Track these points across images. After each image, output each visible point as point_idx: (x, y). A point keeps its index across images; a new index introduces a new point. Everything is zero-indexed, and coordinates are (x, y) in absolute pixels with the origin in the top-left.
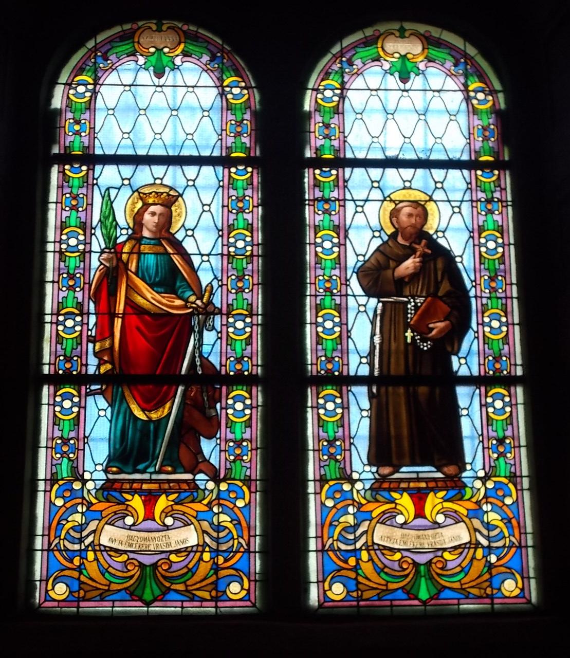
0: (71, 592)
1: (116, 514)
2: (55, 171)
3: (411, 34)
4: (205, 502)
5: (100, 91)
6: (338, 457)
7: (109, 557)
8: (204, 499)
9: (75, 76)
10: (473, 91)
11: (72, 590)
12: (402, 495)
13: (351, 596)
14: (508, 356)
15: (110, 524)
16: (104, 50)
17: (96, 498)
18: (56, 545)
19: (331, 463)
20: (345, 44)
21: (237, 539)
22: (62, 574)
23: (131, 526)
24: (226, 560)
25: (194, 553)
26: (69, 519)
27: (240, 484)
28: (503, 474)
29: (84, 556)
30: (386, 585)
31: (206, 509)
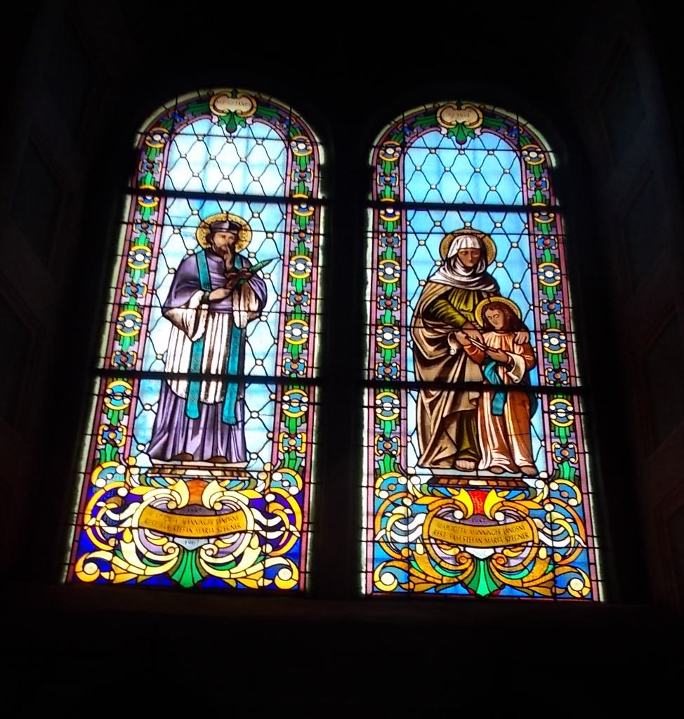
0: (399, 584)
1: (516, 512)
2: (129, 199)
3: (244, 96)
4: (538, 500)
5: (175, 139)
6: (394, 453)
7: (438, 549)
8: (536, 497)
9: (385, 141)
10: (295, 141)
11: (400, 581)
12: (459, 491)
13: (401, 587)
14: (398, 363)
15: (438, 517)
16: (409, 122)
17: (421, 493)
18: (382, 537)
19: (386, 458)
20: (406, 114)
21: (574, 537)
22: (389, 564)
23: (460, 520)
24: (564, 557)
25: (529, 549)
26: (394, 512)
27: (293, 473)
28: (566, 476)
29: (413, 549)
30: (442, 580)
31: (540, 507)
